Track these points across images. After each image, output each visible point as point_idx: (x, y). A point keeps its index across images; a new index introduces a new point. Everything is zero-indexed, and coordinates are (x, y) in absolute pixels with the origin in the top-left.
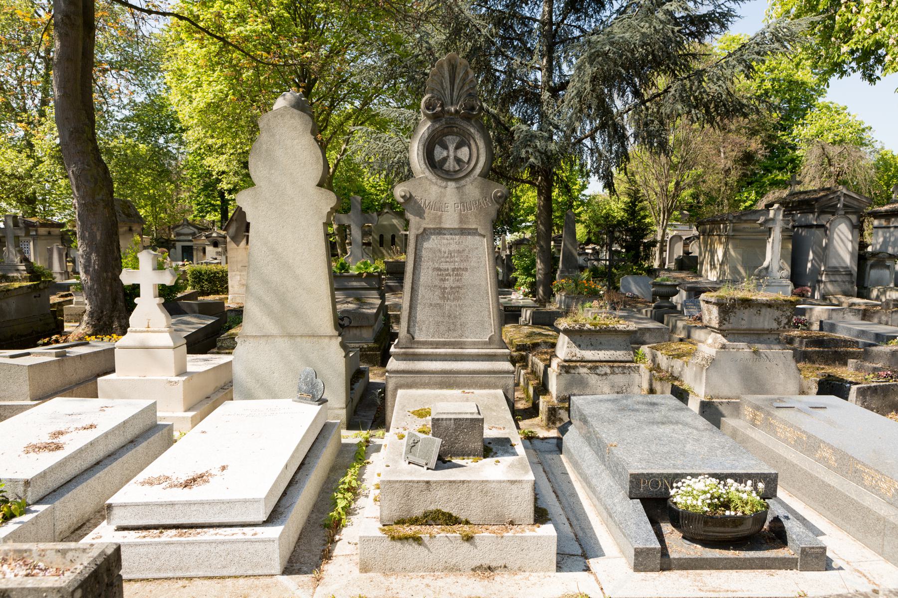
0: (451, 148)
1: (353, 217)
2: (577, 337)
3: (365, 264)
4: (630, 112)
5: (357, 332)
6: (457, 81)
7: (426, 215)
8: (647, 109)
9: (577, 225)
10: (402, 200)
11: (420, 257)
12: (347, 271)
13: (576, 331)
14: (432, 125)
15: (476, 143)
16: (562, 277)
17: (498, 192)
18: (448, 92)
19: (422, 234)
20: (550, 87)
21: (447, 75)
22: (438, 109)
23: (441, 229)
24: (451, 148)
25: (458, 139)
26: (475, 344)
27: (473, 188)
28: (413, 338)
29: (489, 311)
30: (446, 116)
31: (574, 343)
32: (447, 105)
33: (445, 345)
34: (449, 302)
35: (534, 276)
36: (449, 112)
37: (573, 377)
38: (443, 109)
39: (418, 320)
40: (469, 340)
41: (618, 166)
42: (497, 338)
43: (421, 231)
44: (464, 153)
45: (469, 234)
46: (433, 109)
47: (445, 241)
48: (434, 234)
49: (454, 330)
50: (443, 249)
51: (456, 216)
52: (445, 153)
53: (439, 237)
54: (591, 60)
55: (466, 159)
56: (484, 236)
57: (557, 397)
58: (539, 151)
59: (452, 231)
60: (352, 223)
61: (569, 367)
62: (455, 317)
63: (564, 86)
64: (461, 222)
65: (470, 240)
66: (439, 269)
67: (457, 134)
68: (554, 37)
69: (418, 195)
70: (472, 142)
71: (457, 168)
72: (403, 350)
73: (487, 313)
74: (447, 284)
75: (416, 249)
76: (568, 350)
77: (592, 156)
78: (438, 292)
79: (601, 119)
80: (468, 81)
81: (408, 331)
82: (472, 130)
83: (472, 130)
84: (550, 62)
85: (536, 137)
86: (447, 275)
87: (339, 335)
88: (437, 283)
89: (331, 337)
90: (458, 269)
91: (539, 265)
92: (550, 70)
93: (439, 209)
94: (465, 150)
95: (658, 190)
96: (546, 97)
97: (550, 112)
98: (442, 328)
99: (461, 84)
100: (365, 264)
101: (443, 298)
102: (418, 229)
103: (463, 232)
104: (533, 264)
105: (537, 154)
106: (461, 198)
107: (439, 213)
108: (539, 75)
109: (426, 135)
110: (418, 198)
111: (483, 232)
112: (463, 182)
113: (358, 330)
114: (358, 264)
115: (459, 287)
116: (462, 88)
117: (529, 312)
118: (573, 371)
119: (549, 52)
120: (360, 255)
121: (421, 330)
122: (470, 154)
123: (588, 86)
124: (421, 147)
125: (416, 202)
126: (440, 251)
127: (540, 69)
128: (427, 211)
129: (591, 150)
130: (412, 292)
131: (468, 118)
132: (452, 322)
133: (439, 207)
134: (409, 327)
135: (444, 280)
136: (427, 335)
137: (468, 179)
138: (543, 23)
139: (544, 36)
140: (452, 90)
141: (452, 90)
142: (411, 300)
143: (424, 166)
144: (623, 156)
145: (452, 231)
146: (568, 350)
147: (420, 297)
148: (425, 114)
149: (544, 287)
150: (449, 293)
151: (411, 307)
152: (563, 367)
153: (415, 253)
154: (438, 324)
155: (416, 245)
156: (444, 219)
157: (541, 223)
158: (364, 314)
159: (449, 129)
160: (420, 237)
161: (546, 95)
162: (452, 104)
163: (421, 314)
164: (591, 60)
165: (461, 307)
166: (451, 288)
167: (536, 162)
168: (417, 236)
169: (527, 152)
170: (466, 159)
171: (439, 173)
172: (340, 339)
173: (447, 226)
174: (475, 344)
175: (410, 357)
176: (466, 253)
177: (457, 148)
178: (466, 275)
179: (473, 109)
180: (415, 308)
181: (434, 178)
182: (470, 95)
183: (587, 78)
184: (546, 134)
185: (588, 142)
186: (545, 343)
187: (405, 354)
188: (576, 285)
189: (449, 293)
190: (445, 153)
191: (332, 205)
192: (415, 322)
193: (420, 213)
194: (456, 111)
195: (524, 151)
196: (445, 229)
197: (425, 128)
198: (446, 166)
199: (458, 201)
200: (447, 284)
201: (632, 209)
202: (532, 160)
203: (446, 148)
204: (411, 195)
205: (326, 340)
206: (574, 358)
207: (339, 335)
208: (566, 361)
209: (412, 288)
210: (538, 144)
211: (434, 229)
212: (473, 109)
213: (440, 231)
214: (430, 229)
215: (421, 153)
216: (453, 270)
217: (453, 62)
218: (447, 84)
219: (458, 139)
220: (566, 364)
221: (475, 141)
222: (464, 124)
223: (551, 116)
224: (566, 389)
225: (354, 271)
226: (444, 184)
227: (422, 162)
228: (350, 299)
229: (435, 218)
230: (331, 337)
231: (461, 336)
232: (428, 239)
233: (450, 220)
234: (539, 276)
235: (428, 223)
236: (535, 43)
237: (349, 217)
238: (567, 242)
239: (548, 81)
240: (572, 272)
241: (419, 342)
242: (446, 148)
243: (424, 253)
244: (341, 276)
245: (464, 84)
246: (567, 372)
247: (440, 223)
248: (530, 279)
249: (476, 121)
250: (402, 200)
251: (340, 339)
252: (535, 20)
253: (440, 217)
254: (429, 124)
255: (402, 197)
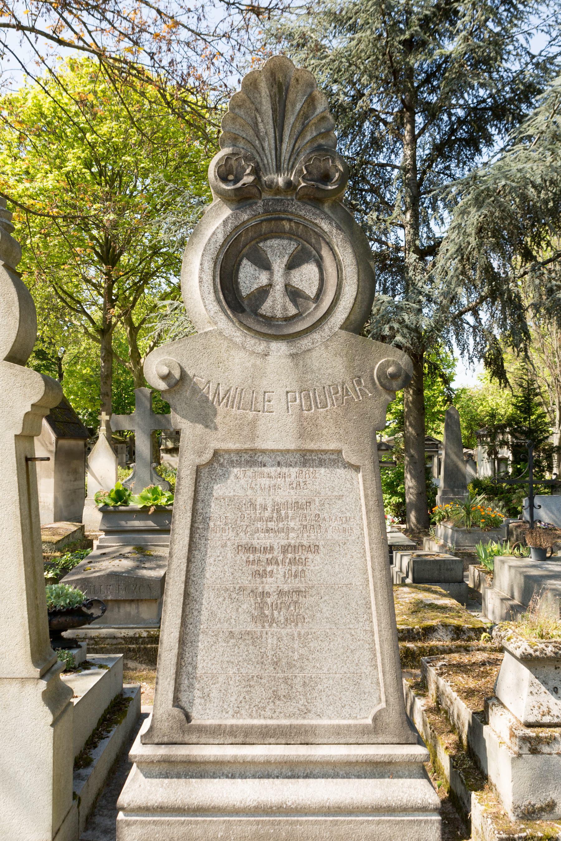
0: (278, 266)
1: (137, 419)
2: (550, 670)
3: (154, 491)
4: (527, 277)
5: (131, 609)
6: (291, 119)
7: (218, 420)
8: (550, 272)
9: (167, 388)
10: (162, 386)
11: (206, 520)
12: (126, 503)
13: (549, 659)
14: (235, 216)
15: (335, 255)
16: (445, 500)
17: (387, 364)
18: (269, 144)
19: (210, 463)
20: (416, 247)
21: (266, 106)
22: (248, 179)
23: (254, 451)
24: (278, 266)
25: (292, 247)
26: (339, 734)
27: (329, 355)
28: (188, 718)
29: (373, 651)
30: (265, 196)
31: (544, 683)
32: (267, 171)
33: (266, 735)
34: (275, 628)
35: (403, 495)
36: (271, 186)
37: (546, 762)
38: (258, 178)
39: (199, 672)
40: (325, 722)
41: (517, 346)
42: (393, 718)
43: (207, 456)
44: (306, 277)
45: (321, 463)
46: (236, 181)
47: (265, 482)
48: (239, 464)
49: (288, 697)
50: (260, 500)
51: (290, 422)
52: (263, 278)
53: (250, 472)
54: (479, 203)
55: (311, 291)
56: (357, 468)
57: (516, 808)
58: (407, 327)
59: (281, 458)
60: (136, 428)
61: (539, 740)
62: (290, 665)
63: (433, 250)
64: (302, 434)
65: (324, 478)
66: (252, 549)
67: (291, 235)
68: (420, 184)
69: (199, 373)
70: (325, 253)
71: (292, 311)
72: (162, 751)
73: (368, 655)
74: (270, 585)
75: (195, 500)
76: (532, 700)
77: (475, 336)
78: (248, 604)
79: (490, 284)
80: (314, 119)
81: (176, 702)
82: (325, 226)
83: (325, 226)
84: (415, 216)
85: (402, 309)
86: (269, 562)
87: (42, 677)
88: (246, 581)
89: (23, 680)
90: (295, 549)
91: (410, 482)
92: (415, 226)
93: (251, 406)
94: (309, 270)
95: (550, 379)
96: (412, 261)
97: (418, 278)
98: (259, 693)
99: (299, 127)
100: (154, 491)
101: (261, 618)
102: (200, 453)
103: (307, 458)
104: (400, 478)
105: (405, 331)
106: (301, 380)
107: (251, 415)
108: (401, 233)
109: (220, 238)
110: (200, 381)
111: (353, 460)
112: (305, 343)
113: (134, 606)
114: (144, 492)
115: (298, 592)
116: (301, 134)
117: (406, 560)
118: (545, 749)
119: (414, 203)
120: (147, 477)
121: (206, 697)
122: (322, 280)
123: (473, 241)
124: (208, 265)
125: (195, 390)
126: (253, 505)
127: (402, 226)
128: (221, 409)
129: (474, 328)
130: (185, 605)
131: (315, 199)
132: (283, 677)
133: (250, 400)
134: (177, 690)
135: (261, 575)
136: (223, 710)
137: (316, 336)
138: (405, 170)
139: (407, 185)
140: (279, 140)
141: (279, 140)
142: (184, 623)
143: (214, 307)
144: (519, 335)
145: (281, 458)
146: (532, 700)
147: (205, 615)
148: (221, 193)
149: (417, 511)
150: (276, 607)
151: (182, 642)
152: (525, 739)
153: (194, 511)
154: (249, 682)
155: (196, 491)
156: (261, 429)
157: (411, 425)
158: (142, 579)
159: (273, 224)
160: (205, 472)
161: (412, 258)
162: (278, 170)
163: (209, 657)
164: (479, 203)
165: (303, 638)
166: (281, 593)
167: (403, 341)
168: (198, 470)
169: (391, 328)
170: (311, 291)
171: (250, 322)
172: (43, 685)
173: (269, 445)
174: (339, 734)
175: (180, 768)
176: (314, 509)
177: (292, 265)
178: (316, 563)
179: (326, 178)
180: (194, 643)
181: (236, 334)
182: (319, 148)
183: (471, 230)
184: (416, 306)
185: (469, 318)
186: (445, 626)
187: (167, 761)
188: (468, 513)
189: (276, 607)
190: (263, 278)
191: (36, 399)
192: (192, 677)
193: (205, 415)
194: (289, 184)
195: (387, 327)
196: (263, 452)
197: (218, 220)
198: (266, 308)
199: (295, 386)
200: (270, 585)
201: (526, 405)
202: (398, 338)
203: (266, 266)
204: (183, 374)
205: (14, 688)
206: (547, 719)
207: (42, 677)
208: (529, 725)
209: (186, 595)
210: (406, 317)
211: (238, 452)
212: (326, 178)
213: (251, 458)
214: (228, 451)
215: (208, 278)
216: (285, 550)
217: (280, 77)
218: (267, 126)
219: (292, 247)
220: (531, 733)
221: (332, 249)
222: (306, 212)
223: (420, 284)
224: (534, 790)
225: (136, 503)
226: (261, 346)
227: (212, 297)
228: (128, 549)
229: (241, 427)
230: (23, 680)
231: (305, 713)
232: (225, 476)
233: (277, 432)
234: (410, 498)
235: (223, 439)
236: (396, 194)
237: (132, 419)
238: (450, 451)
239: (414, 240)
240: (458, 493)
241: (201, 730)
242: (266, 266)
243: (215, 510)
244: (116, 512)
245: (304, 127)
246: (534, 751)
247: (253, 437)
248: (396, 500)
249: (335, 206)
250: (162, 386)
251: (43, 685)
252: (394, 167)
253: (253, 424)
254: (227, 212)
255: (165, 378)
